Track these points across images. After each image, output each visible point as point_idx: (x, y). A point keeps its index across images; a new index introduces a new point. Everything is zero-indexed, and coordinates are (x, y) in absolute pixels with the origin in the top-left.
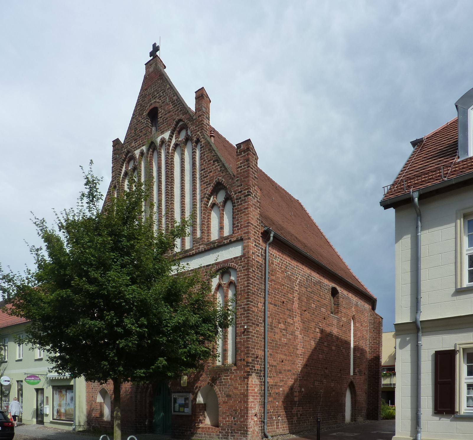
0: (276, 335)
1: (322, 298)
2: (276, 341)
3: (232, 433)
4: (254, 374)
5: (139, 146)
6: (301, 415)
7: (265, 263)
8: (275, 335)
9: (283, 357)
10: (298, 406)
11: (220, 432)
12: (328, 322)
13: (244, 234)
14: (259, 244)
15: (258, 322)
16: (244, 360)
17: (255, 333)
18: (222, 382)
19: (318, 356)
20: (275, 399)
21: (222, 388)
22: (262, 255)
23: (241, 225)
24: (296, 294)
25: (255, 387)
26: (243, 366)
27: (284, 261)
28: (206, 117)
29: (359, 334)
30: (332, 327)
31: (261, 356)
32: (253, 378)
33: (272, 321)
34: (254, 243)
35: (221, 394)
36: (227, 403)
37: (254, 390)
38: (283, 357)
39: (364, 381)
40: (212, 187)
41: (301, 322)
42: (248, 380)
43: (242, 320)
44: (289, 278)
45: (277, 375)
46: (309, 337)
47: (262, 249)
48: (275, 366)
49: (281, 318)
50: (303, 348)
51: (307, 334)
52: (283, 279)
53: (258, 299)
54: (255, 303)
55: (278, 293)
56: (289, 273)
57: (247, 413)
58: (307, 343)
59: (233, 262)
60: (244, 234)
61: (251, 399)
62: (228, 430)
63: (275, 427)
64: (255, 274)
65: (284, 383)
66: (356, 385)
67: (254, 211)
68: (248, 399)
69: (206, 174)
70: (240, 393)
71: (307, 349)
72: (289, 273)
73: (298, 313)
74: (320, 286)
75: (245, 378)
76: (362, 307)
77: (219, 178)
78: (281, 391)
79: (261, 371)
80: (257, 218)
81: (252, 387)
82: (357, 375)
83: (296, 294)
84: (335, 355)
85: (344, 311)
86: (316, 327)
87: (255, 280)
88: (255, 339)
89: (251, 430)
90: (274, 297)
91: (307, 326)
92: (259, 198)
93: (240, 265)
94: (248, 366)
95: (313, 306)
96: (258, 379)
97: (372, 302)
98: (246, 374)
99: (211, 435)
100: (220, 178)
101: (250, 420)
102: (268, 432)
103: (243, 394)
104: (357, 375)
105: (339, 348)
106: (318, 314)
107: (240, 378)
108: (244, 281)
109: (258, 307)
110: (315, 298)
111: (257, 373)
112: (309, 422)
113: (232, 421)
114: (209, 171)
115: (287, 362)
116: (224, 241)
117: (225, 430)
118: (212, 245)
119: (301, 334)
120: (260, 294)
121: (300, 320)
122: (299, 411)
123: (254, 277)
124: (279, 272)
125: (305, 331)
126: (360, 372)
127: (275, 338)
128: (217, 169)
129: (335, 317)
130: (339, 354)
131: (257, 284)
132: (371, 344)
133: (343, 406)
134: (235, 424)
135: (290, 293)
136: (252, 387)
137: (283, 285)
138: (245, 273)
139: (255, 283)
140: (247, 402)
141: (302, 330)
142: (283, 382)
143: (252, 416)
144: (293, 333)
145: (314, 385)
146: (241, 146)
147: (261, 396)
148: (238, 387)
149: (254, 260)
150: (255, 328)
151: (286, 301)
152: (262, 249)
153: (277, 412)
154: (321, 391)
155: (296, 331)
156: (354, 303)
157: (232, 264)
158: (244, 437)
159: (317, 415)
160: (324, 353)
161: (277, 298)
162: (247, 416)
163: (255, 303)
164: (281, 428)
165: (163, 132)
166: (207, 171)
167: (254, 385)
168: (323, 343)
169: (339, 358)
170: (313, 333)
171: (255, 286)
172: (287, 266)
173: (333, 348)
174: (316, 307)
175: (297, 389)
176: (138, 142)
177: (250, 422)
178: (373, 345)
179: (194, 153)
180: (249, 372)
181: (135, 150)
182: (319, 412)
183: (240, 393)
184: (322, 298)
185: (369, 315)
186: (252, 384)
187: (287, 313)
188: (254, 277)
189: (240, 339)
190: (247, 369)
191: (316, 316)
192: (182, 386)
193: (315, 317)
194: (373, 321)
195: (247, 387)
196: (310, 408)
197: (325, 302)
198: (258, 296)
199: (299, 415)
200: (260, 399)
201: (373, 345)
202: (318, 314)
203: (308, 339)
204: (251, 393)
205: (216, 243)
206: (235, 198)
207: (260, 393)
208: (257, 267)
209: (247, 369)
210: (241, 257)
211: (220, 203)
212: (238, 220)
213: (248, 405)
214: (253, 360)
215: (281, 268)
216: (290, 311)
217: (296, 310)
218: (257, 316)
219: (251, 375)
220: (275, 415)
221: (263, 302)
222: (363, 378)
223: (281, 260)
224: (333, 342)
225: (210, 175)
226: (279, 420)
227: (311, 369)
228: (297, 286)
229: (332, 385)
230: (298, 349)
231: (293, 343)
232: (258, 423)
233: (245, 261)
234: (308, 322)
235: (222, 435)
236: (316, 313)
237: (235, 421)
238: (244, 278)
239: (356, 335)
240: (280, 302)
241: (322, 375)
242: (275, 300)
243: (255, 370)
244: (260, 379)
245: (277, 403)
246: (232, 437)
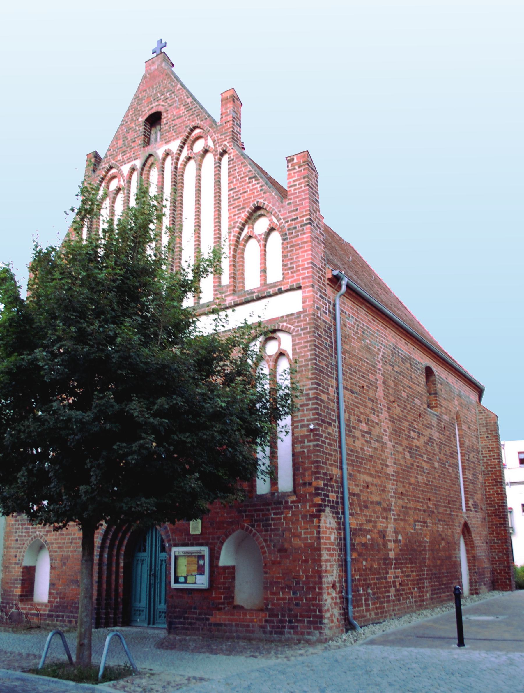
0: (357, 441)
1: (414, 383)
2: (357, 452)
3: (290, 621)
4: (328, 509)
5: (129, 160)
6: (400, 584)
7: (335, 325)
8: (354, 442)
9: (369, 479)
10: (396, 568)
11: (266, 621)
12: (425, 422)
13: (303, 279)
14: (326, 295)
15: (330, 419)
16: (310, 484)
17: (326, 438)
18: (270, 525)
19: (417, 478)
20: (360, 554)
21: (270, 536)
22: (330, 312)
23: (298, 266)
24: (379, 375)
25: (331, 533)
26: (309, 496)
27: (360, 322)
28: (237, 124)
29: (467, 443)
30: (432, 429)
31: (336, 477)
32: (326, 517)
33: (350, 418)
34: (319, 294)
35: (268, 546)
36: (279, 563)
37: (329, 538)
38: (369, 479)
39: (482, 522)
40: (248, 212)
41: (390, 421)
42: (320, 520)
43: (304, 415)
44: (368, 349)
45: (361, 510)
46: (401, 445)
47: (330, 303)
48: (358, 495)
49: (361, 413)
50: (395, 463)
51: (399, 440)
52: (360, 351)
53: (328, 380)
54: (324, 387)
55: (355, 372)
56: (368, 341)
57: (321, 583)
58: (400, 455)
59: (286, 321)
60: (303, 279)
61: (325, 556)
62: (283, 616)
63: (364, 608)
64: (322, 341)
65: (373, 526)
66: (472, 529)
67: (317, 247)
68: (320, 555)
69: (236, 195)
70: (305, 544)
71: (401, 465)
72: (368, 341)
73: (384, 406)
74: (410, 364)
75: (313, 516)
76: (467, 399)
77: (259, 200)
78: (369, 540)
79: (337, 503)
80: (321, 257)
81: (325, 532)
82: (471, 511)
83: (379, 375)
84: (439, 476)
85: (444, 403)
86: (409, 429)
87: (322, 350)
88: (326, 448)
89: (327, 615)
90: (351, 379)
91: (399, 428)
92: (322, 228)
93: (297, 326)
94: (318, 494)
95: (404, 395)
96: (334, 518)
97: (479, 390)
98: (314, 509)
99: (248, 626)
100: (261, 200)
101: (325, 596)
102: (355, 618)
103: (311, 545)
104: (471, 511)
105: (443, 464)
106: (411, 408)
107: (304, 517)
108: (305, 352)
109: (328, 394)
110: (406, 382)
111: (332, 507)
112: (412, 598)
113: (290, 599)
114: (241, 192)
115: (374, 488)
116: (269, 290)
117: (277, 616)
118: (247, 296)
119: (390, 441)
120: (331, 372)
121: (388, 417)
122: (397, 577)
123: (321, 345)
124: (354, 339)
125: (396, 435)
126: (475, 505)
127: (355, 446)
128: (256, 188)
129: (433, 414)
130: (444, 475)
131: (326, 356)
132: (485, 459)
133: (456, 565)
134: (297, 605)
135: (372, 373)
136: (325, 532)
137: (361, 360)
138: (306, 338)
139: (322, 354)
140: (320, 560)
141: (392, 434)
142: (371, 524)
143: (328, 587)
144: (379, 440)
145: (415, 529)
146: (293, 159)
147: (341, 550)
148: (301, 533)
149: (320, 319)
150: (326, 428)
151: (367, 386)
152: (330, 303)
153: (365, 580)
154: (426, 539)
155: (383, 434)
156: (456, 392)
157: (283, 326)
158: (315, 629)
159: (424, 583)
160: (424, 473)
161: (355, 380)
162: (320, 588)
163: (324, 387)
164: (373, 609)
165: (169, 141)
166: (239, 191)
167: (329, 529)
168: (422, 456)
169: (445, 482)
170: (406, 439)
171: (323, 359)
172: (364, 330)
173: (436, 465)
174: (407, 396)
175: (392, 537)
176: (128, 155)
177: (326, 600)
178: (488, 460)
179: (218, 167)
180: (320, 505)
181: (122, 165)
182: (426, 579)
183: (305, 544)
184: (414, 383)
185: (477, 412)
186: (326, 528)
187: (370, 404)
188: (321, 345)
189: (302, 447)
190: (317, 500)
191: (409, 411)
192: (192, 532)
193: (407, 414)
194: (484, 422)
195: (319, 533)
196: (412, 572)
197: (418, 389)
198: (328, 375)
199: (397, 584)
200: (339, 555)
201: (488, 460)
202: (411, 408)
203: (400, 449)
204: (325, 544)
205: (254, 292)
206: (286, 228)
207: (338, 544)
208: (325, 330)
209: (317, 500)
210: (299, 313)
211: (260, 235)
212: (291, 259)
213: (320, 566)
214: (325, 485)
215: (357, 333)
216: (373, 401)
217: (381, 401)
218: (328, 408)
219: (324, 511)
220: (363, 586)
221: (335, 386)
222: (480, 515)
223: (356, 320)
224: (434, 454)
225: (244, 196)
226: (368, 594)
227: (408, 500)
228: (379, 362)
229: (440, 528)
230: (387, 466)
231: (381, 455)
232: (338, 601)
233: (306, 320)
234: (400, 421)
235: (272, 627)
236: (409, 406)
237: (296, 599)
238: (306, 347)
239: (463, 444)
240: (359, 387)
241: (424, 511)
242: (351, 383)
243: (329, 501)
244: (338, 518)
245: (364, 563)
246: (292, 631)
